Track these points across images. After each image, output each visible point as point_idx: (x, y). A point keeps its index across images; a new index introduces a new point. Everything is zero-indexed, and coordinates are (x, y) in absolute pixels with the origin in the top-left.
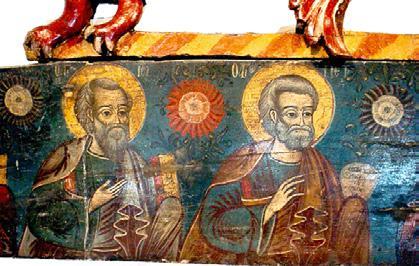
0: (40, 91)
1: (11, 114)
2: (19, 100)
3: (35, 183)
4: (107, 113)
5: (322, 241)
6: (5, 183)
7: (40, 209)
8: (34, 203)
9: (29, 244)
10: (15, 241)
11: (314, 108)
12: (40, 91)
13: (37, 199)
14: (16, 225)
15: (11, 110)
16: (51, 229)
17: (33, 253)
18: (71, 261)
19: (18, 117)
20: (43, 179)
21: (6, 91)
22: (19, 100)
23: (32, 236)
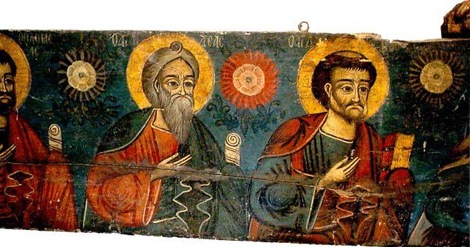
0: (462, 67)
1: (425, 91)
2: (436, 76)
3: (442, 167)
4: (173, 84)
5: (188, 189)
6: (407, 166)
7: (443, 194)
8: (437, 186)
9: (422, 232)
10: (406, 229)
11: (194, 75)
12: (462, 67)
13: (441, 183)
14: (411, 211)
15: (426, 87)
16: (451, 215)
17: (426, 240)
18: (34, 234)
19: (434, 95)
20: (458, 160)
21: (423, 66)
22: (436, 76)
23: (427, 221)
